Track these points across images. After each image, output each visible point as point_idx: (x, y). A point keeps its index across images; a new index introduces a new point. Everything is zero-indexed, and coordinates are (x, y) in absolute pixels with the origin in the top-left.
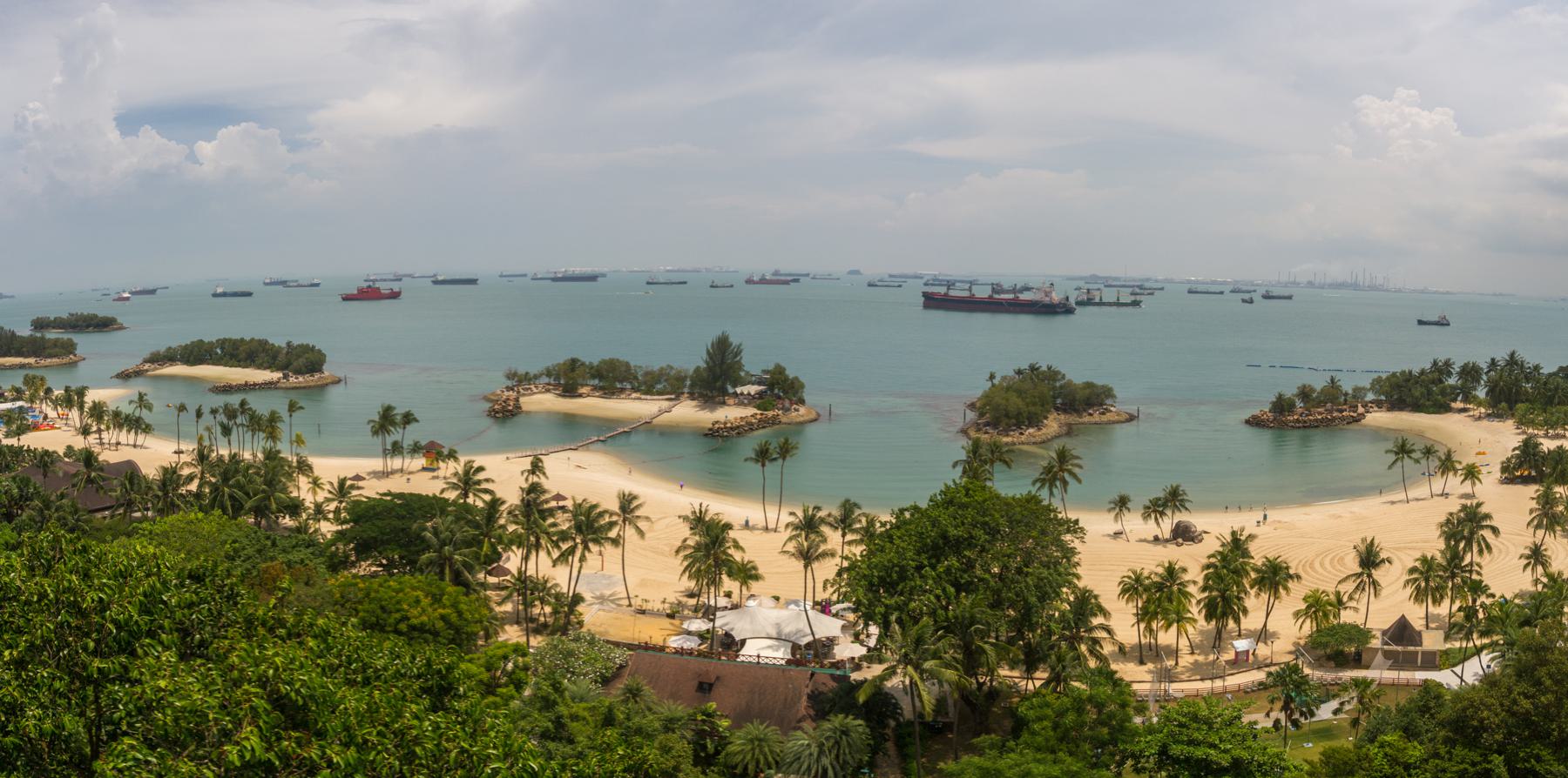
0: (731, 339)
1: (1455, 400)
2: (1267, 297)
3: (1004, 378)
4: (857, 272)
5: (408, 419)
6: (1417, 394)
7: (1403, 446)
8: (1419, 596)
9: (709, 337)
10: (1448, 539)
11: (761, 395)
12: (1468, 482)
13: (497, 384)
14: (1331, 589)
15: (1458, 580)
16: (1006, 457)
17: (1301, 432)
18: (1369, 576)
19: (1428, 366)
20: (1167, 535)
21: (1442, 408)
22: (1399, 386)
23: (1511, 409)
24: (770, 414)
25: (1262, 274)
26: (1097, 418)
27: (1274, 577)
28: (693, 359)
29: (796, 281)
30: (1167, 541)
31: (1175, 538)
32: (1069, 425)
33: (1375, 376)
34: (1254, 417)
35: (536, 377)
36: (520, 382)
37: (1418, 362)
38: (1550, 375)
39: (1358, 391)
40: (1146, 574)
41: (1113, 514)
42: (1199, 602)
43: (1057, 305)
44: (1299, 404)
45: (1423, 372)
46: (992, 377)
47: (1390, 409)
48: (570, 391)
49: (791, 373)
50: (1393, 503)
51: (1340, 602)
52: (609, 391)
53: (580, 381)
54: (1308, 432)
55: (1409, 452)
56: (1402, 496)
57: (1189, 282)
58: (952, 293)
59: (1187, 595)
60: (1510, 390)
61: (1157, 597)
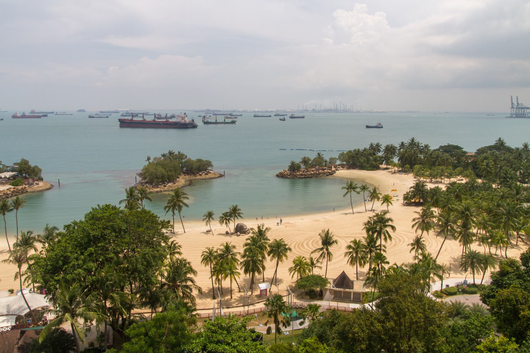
1: (382, 164)
2: (292, 117)
3: (155, 159)
4: (83, 111)
6: (362, 161)
7: (351, 185)
8: (353, 261)
10: (368, 231)
11: (14, 177)
12: (385, 204)
14: (307, 256)
15: (373, 254)
16: (149, 196)
17: (304, 180)
18: (327, 249)
19: (368, 147)
20: (233, 231)
21: (375, 167)
22: (353, 157)
23: (411, 168)
24: (20, 187)
25: (290, 106)
26: (203, 176)
27: (279, 250)
29: (46, 116)
30: (232, 234)
31: (236, 232)
32: (191, 181)
33: (341, 152)
34: (281, 173)
37: (363, 145)
38: (435, 150)
39: (332, 160)
40: (215, 250)
41: (205, 222)
42: (241, 263)
43: (189, 124)
44: (303, 167)
45: (365, 150)
46: (149, 159)
47: (348, 169)
49: (32, 164)
50: (346, 214)
51: (312, 263)
54: (309, 179)
55: (354, 188)
56: (351, 211)
57: (255, 111)
58: (135, 119)
59: (236, 260)
60: (411, 158)
61: (221, 262)
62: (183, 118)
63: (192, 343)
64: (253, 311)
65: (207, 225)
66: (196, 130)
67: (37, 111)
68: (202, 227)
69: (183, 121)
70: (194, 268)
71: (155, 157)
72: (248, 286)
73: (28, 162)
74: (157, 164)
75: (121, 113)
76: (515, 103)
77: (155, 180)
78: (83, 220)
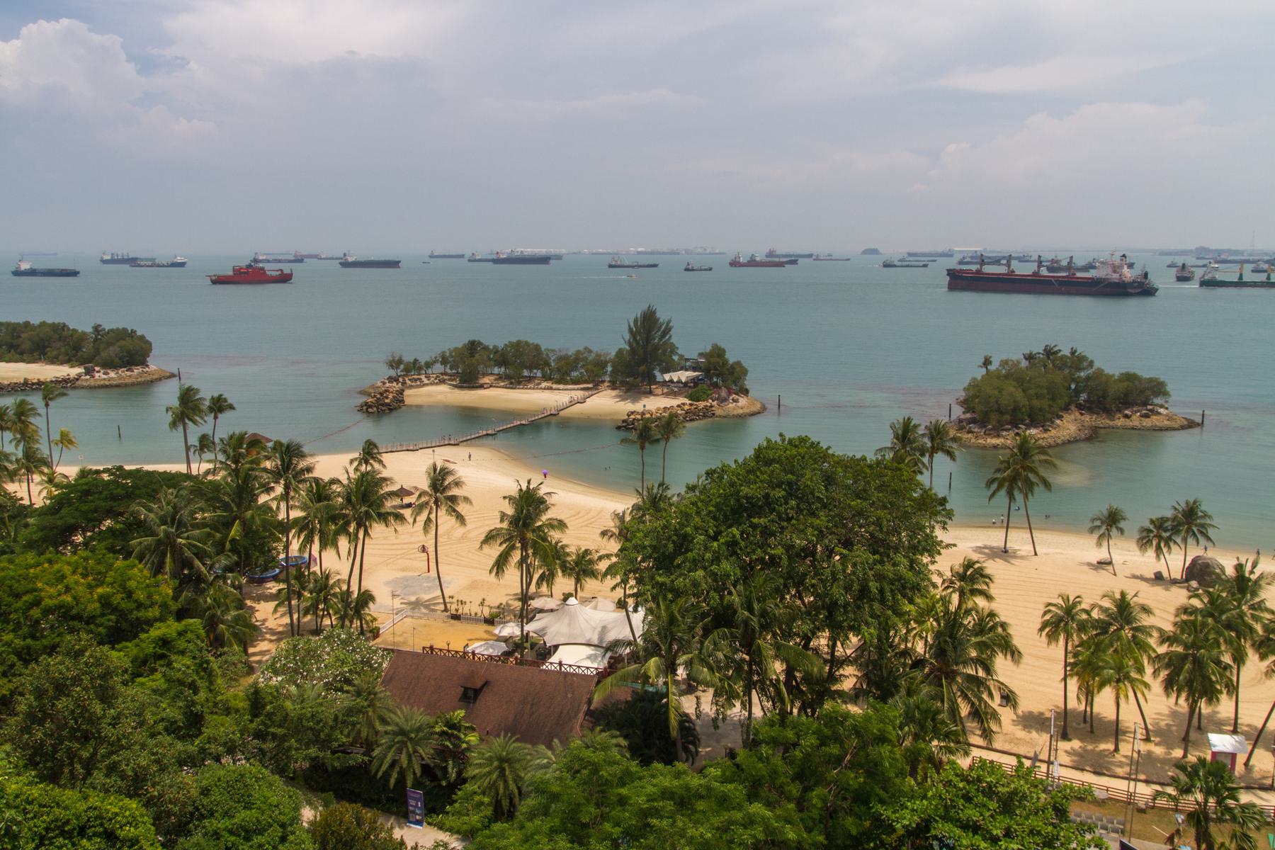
0: (658, 315)
3: (1004, 363)
4: (874, 251)
5: (219, 406)
9: (636, 311)
11: (695, 381)
13: (378, 376)
24: (701, 404)
26: (1136, 421)
28: (612, 340)
29: (794, 262)
30: (1174, 582)
31: (1187, 580)
35: (428, 365)
36: (407, 370)
41: (1096, 535)
43: (1131, 284)
46: (987, 362)
48: (468, 380)
49: (731, 358)
52: (515, 380)
53: (481, 368)
58: (988, 269)
61: (1099, 642)
62: (1115, 269)
63: (903, 807)
64: (1124, 797)
65: (1099, 544)
66: (1149, 301)
67: (778, 253)
68: (1087, 549)
69: (1116, 276)
70: (1016, 642)
71: (1004, 358)
72: (1178, 732)
73: (724, 351)
74: (1006, 377)
75: (958, 257)
77: (994, 417)
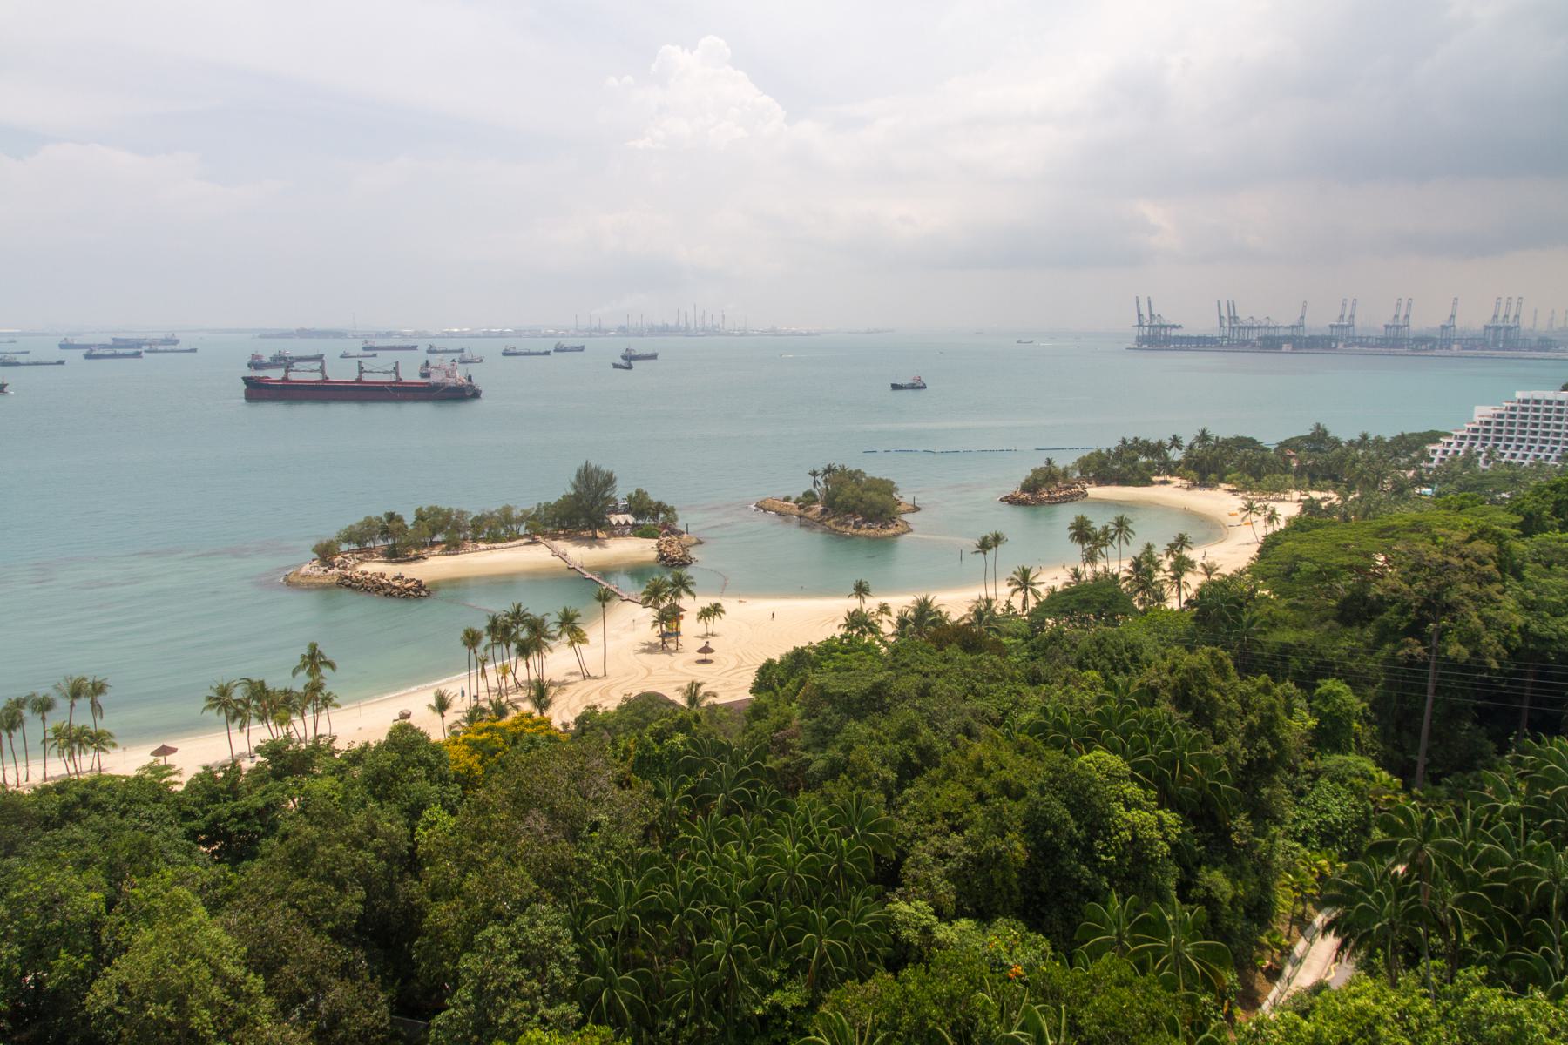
9: (1201, 428)
27: (96, 709)
52: (453, 547)
58: (293, 376)
66: (475, 405)
76: (1147, 316)
78: (778, 660)
